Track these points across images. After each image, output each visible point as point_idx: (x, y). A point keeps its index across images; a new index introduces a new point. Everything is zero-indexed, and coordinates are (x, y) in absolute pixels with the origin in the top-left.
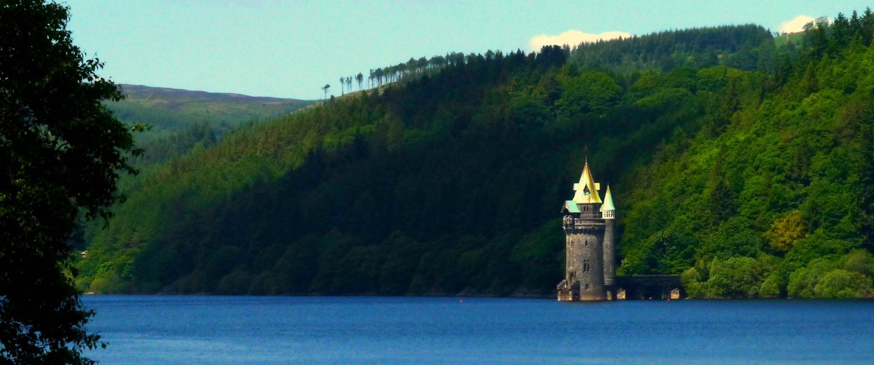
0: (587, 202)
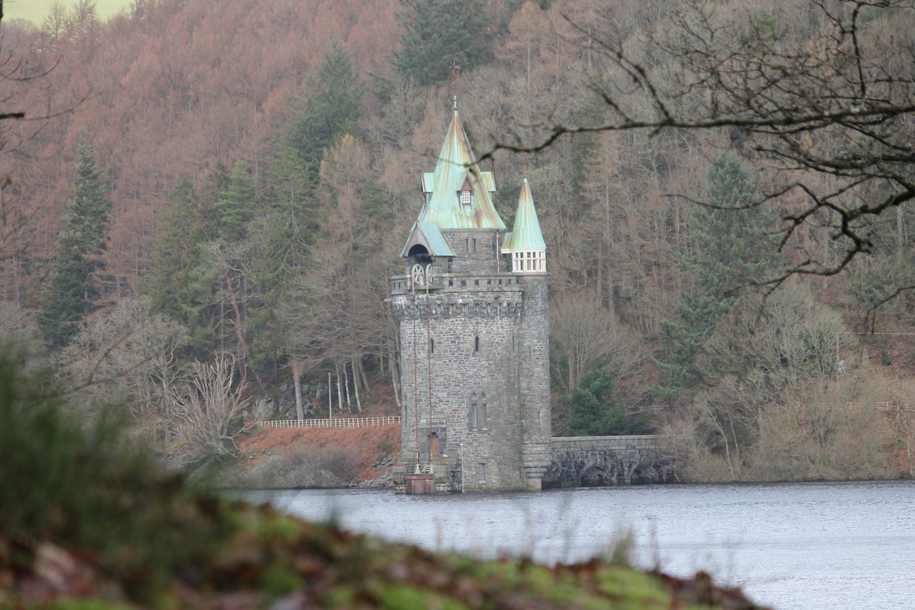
0: (471, 225)
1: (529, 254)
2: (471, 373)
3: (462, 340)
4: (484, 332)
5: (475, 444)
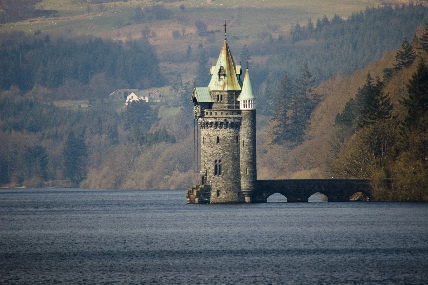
0: (220, 89)
2: (215, 151)
4: (221, 134)
5: (216, 181)
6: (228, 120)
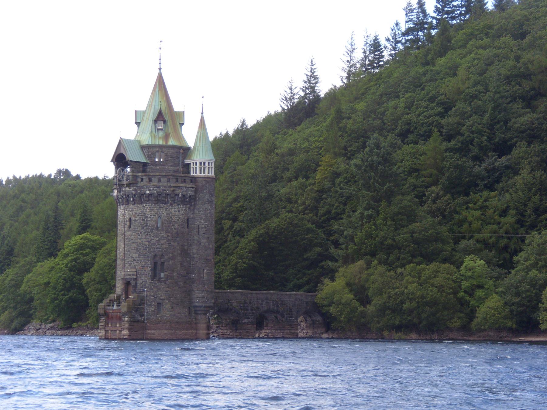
0: (161, 142)
1: (201, 163)
2: (154, 241)
3: (149, 219)
4: (165, 214)
6: (178, 191)
